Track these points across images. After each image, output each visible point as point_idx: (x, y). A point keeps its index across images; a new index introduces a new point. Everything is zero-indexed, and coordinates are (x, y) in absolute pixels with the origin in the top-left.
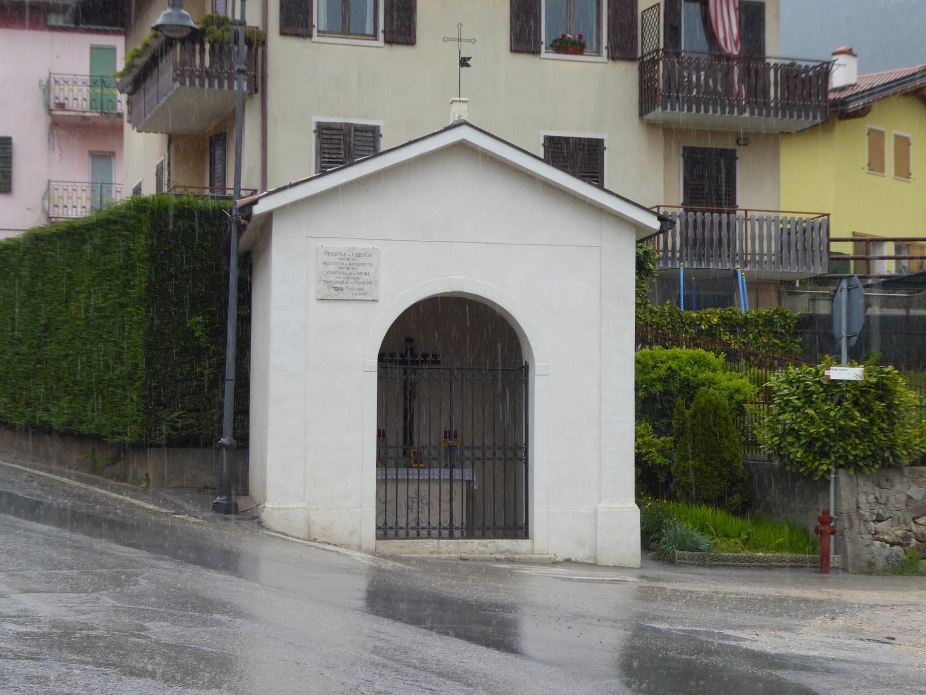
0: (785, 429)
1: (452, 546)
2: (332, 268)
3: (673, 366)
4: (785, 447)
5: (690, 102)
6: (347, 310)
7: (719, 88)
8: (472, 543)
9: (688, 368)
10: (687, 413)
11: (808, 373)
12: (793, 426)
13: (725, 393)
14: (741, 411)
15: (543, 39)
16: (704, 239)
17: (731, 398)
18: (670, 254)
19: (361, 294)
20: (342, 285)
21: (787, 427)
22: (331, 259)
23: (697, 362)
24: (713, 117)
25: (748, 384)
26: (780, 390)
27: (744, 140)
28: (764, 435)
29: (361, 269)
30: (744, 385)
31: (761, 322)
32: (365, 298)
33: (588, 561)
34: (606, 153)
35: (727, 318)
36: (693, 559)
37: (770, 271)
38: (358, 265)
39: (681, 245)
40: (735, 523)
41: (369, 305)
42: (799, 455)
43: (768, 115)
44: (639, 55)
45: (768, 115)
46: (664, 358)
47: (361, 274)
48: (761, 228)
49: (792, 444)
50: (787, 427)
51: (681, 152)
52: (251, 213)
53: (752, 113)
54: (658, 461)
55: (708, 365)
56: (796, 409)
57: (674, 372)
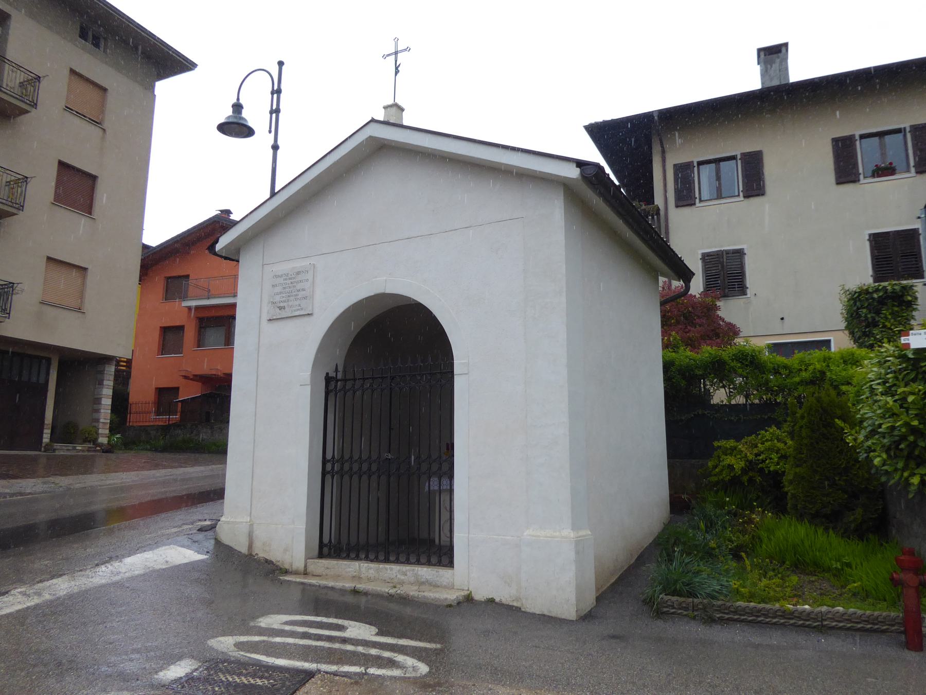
1: (371, 571)
6: (288, 329)
15: (861, 171)
20: (285, 304)
29: (299, 286)
36: (686, 609)
38: (297, 282)
41: (306, 319)
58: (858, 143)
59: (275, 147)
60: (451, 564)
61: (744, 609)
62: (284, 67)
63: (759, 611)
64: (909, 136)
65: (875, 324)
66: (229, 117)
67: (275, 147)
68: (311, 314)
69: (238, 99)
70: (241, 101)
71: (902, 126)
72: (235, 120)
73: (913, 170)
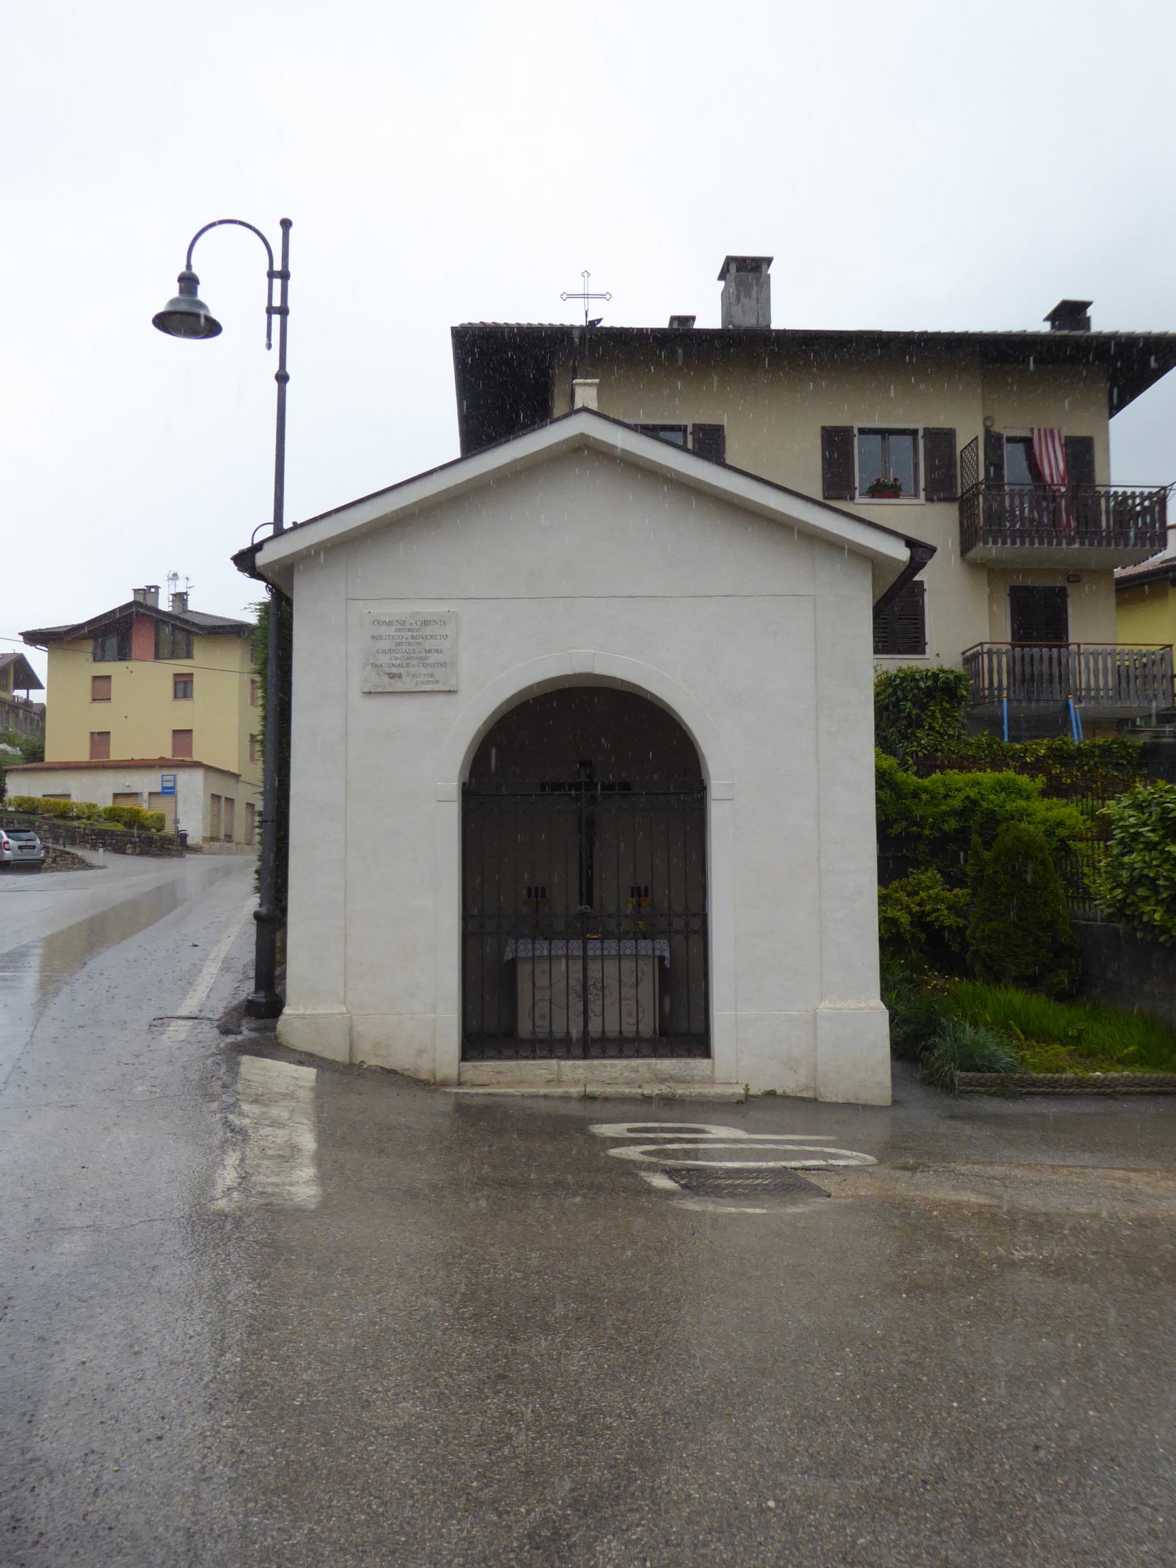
0: (1132, 877)
2: (384, 645)
3: (972, 795)
4: (1132, 903)
5: (1014, 535)
6: (407, 711)
7: (1045, 520)
8: (613, 1066)
9: (992, 797)
10: (987, 855)
11: (1166, 792)
12: (1146, 871)
13: (1042, 828)
14: (1064, 850)
15: (857, 484)
16: (1033, 674)
17: (1050, 833)
18: (996, 692)
19: (429, 682)
21: (1136, 873)
22: (384, 630)
23: (1005, 788)
24: (1038, 549)
25: (1076, 813)
26: (1122, 819)
27: (1075, 577)
28: (1101, 886)
29: (428, 645)
30: (1070, 816)
31: (1097, 752)
32: (437, 688)
33: (804, 1095)
34: (926, 595)
35: (1055, 749)
37: (1108, 707)
39: (1008, 683)
40: (1060, 1016)
41: (442, 698)
42: (1157, 916)
43: (1100, 544)
44: (959, 494)
45: (1100, 544)
46: (961, 784)
47: (430, 651)
48: (1096, 661)
49: (1145, 899)
50: (1136, 873)
51: (1008, 591)
52: (254, 562)
53: (1082, 544)
54: (947, 923)
55: (1019, 792)
56: (1151, 846)
57: (974, 802)
58: (856, 440)
59: (282, 378)
60: (707, 1053)
61: (1042, 1080)
62: (292, 231)
63: (1057, 1081)
64: (921, 442)
65: (920, 726)
66: (173, 302)
67: (282, 378)
68: (455, 692)
69: (189, 266)
70: (194, 270)
71: (911, 426)
72: (183, 307)
73: (922, 494)
